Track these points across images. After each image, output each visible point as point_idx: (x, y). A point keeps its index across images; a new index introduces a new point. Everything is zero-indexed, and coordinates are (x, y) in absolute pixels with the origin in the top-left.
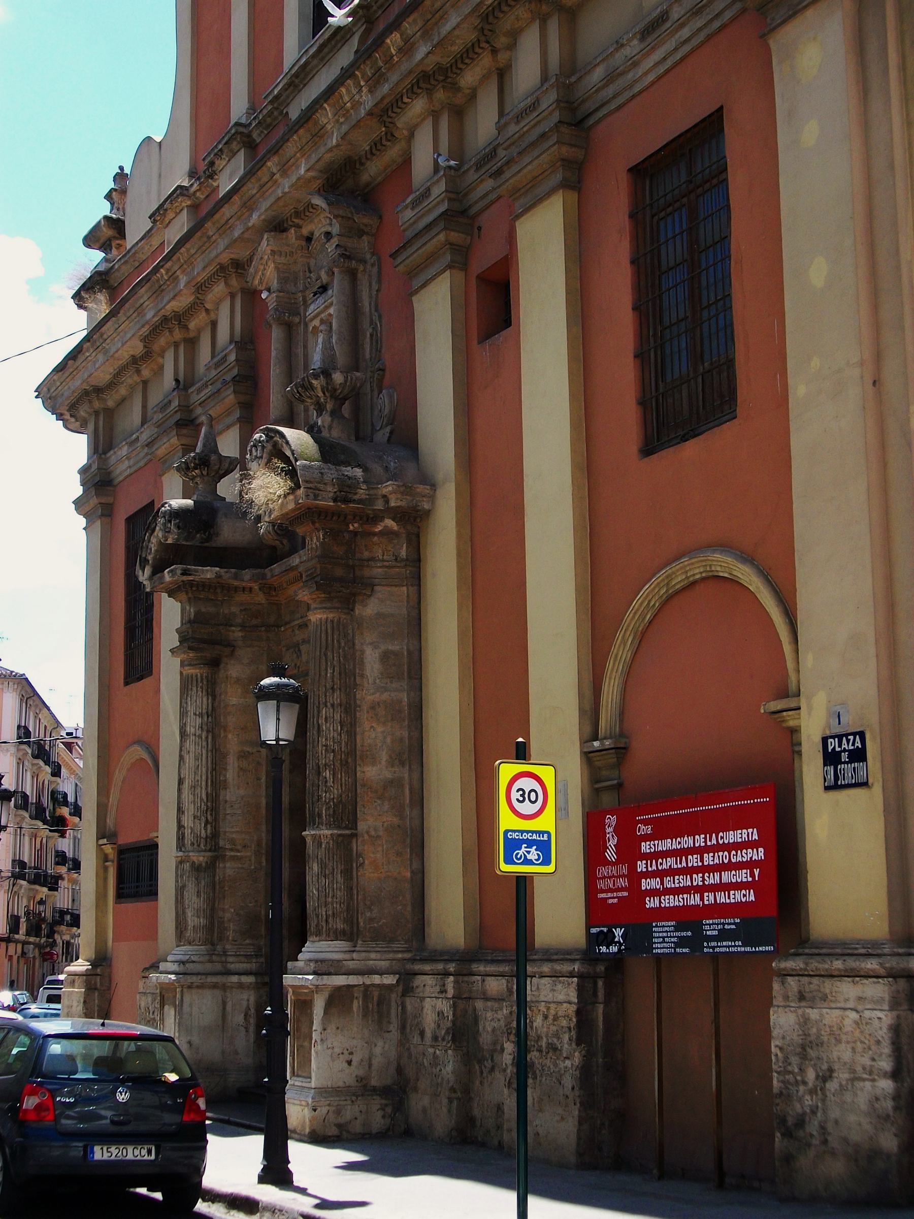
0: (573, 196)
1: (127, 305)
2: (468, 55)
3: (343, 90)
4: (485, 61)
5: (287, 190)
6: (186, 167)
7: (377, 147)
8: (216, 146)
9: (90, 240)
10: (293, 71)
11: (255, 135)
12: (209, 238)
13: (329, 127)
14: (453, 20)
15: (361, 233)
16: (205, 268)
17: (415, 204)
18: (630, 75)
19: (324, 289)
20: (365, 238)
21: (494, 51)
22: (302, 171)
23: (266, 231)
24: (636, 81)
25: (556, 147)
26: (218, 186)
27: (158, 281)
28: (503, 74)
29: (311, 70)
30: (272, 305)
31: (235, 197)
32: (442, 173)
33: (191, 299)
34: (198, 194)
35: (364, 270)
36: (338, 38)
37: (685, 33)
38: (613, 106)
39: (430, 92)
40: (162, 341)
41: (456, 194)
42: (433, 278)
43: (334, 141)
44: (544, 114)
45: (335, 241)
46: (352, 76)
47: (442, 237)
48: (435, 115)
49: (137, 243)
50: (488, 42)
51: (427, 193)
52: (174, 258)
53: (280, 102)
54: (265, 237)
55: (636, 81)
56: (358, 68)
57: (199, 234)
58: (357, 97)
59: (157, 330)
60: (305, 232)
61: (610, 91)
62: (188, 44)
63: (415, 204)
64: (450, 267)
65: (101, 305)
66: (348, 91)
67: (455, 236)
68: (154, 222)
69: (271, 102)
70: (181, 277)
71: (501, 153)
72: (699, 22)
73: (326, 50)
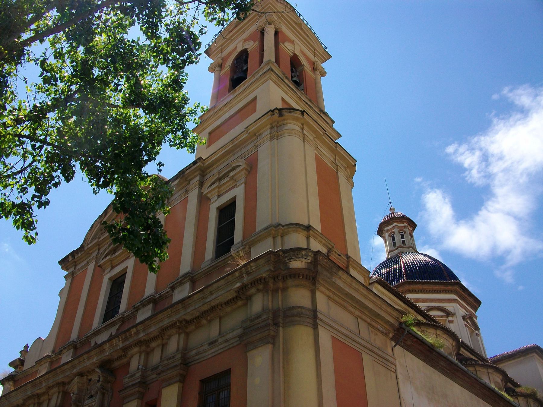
0: (181, 385)
1: (22, 388)
2: (154, 339)
3: (114, 340)
4: (159, 341)
5: (88, 365)
6: (51, 349)
7: (120, 358)
8: (65, 346)
9: (11, 364)
10: (95, 330)
11: (78, 345)
12: (57, 373)
13: (107, 350)
14: (153, 329)
15: (108, 382)
16: (53, 382)
17: (130, 377)
18: (204, 355)
19: (92, 396)
20: (110, 384)
21: (163, 339)
22: (94, 360)
23: (78, 375)
24: (205, 357)
25: (179, 370)
26: (62, 357)
27: (35, 383)
28: (164, 346)
29: (101, 331)
30: (73, 398)
31: (70, 364)
32: (140, 370)
33: (44, 390)
34: (54, 358)
35: (107, 394)
36: (112, 324)
37: (222, 346)
38: (197, 362)
39: (140, 346)
40: (30, 402)
41: (143, 377)
42: (131, 401)
43: (107, 354)
44: (176, 360)
45: (100, 383)
46: (118, 337)
47: (137, 389)
48: (141, 353)
49: (28, 369)
50: (161, 336)
51: (134, 375)
52: (43, 377)
53: (88, 338)
54: (77, 377)
55: (205, 357)
56: (120, 335)
57: (54, 372)
58: (118, 343)
59: (29, 398)
60: (89, 378)
61: (197, 357)
62: (61, 314)
63: (130, 377)
64: (138, 398)
65: (10, 386)
66: (115, 341)
67: (141, 389)
68: (36, 364)
69: (86, 337)
70: (43, 383)
71: (160, 368)
72: (226, 344)
73: (107, 327)
